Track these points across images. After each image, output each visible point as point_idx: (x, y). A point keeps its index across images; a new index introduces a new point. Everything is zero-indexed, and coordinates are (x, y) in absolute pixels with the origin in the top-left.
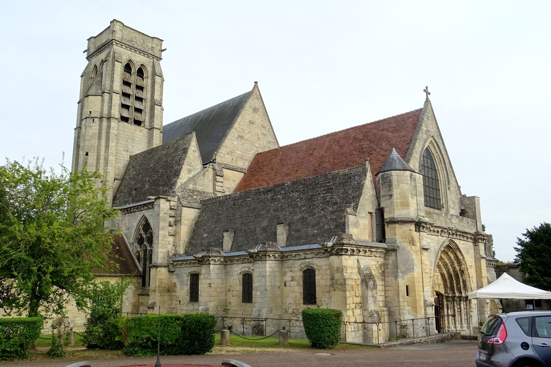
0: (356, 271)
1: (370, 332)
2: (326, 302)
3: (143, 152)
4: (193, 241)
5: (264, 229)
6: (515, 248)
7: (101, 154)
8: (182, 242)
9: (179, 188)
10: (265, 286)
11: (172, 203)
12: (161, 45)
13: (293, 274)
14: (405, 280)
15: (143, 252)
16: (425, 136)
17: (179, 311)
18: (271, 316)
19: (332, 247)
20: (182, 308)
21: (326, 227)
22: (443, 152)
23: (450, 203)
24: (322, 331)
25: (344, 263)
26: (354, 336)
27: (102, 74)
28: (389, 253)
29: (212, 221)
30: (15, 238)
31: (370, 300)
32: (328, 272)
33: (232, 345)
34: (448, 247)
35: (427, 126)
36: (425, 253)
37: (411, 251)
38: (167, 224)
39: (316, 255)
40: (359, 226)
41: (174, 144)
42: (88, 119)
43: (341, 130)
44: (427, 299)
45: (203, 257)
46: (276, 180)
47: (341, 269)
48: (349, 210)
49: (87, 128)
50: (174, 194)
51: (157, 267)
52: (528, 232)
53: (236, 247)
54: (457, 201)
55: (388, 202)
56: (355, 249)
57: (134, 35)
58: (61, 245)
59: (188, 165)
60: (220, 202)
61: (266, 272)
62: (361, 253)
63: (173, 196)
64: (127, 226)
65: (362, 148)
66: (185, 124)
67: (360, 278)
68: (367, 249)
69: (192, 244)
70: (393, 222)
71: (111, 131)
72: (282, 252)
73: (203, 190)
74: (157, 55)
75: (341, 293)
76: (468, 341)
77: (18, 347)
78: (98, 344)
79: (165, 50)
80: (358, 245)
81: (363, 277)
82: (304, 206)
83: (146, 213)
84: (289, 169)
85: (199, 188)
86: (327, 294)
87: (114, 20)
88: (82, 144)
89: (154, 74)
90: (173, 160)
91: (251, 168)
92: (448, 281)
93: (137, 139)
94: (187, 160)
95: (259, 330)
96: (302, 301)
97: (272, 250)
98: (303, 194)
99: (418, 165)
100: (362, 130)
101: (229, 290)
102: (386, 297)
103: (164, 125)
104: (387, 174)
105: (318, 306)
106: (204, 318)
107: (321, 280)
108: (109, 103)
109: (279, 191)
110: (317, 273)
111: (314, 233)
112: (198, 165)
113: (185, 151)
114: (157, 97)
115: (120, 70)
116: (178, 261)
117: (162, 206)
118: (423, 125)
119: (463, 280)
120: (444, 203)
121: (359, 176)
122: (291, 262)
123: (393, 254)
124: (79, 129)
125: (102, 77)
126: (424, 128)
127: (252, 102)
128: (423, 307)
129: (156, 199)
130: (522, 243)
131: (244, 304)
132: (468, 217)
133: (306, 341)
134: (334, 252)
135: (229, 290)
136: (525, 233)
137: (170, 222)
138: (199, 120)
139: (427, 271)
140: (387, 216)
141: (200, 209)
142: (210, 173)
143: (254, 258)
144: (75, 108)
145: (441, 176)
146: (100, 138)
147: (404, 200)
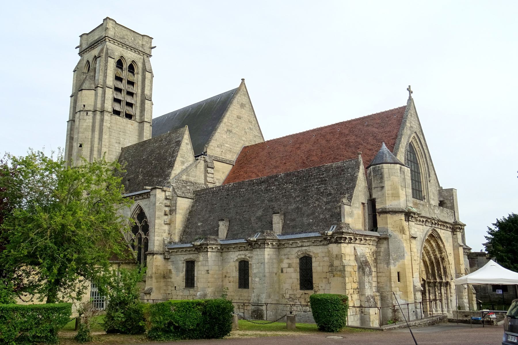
0: (353, 258)
1: (368, 316)
2: (323, 288)
3: (135, 145)
4: (187, 230)
5: (259, 219)
6: (486, 237)
7: (95, 146)
8: (177, 231)
9: (173, 179)
10: (264, 273)
11: (168, 194)
12: (151, 42)
13: (289, 261)
14: (396, 267)
15: (137, 240)
16: (409, 132)
17: (174, 297)
18: (269, 301)
19: (332, 236)
20: (177, 294)
21: (321, 216)
22: (424, 147)
23: (431, 194)
24: (327, 315)
25: (343, 251)
26: (353, 320)
27: (95, 69)
28: (381, 241)
29: (206, 211)
30: (39, 226)
31: (367, 285)
32: (326, 259)
33: (241, 329)
34: (431, 236)
35: (410, 123)
36: (414, 241)
37: (402, 240)
38: (163, 213)
39: (313, 243)
40: (354, 216)
41: (167, 137)
42: (82, 113)
43: (326, 125)
44: (416, 284)
45: (201, 245)
46: (265, 172)
47: (340, 257)
48: (345, 201)
49: (81, 121)
50: (169, 185)
51: (153, 254)
52: (498, 222)
53: (231, 234)
54: (436, 193)
55: (379, 193)
56: (352, 237)
57: (125, 32)
58: (84, 232)
59: (182, 157)
60: (213, 193)
61: (264, 259)
62: (357, 242)
63: (168, 187)
64: (125, 214)
65: (348, 142)
66: (173, 118)
67: (357, 265)
68: (362, 238)
69: (187, 231)
70: (385, 212)
71: (104, 124)
72: (279, 240)
73: (195, 181)
74: (148, 52)
75: (340, 279)
76: (456, 324)
77: (48, 332)
78: (120, 329)
79: (155, 47)
80: (356, 234)
81: (360, 264)
82: (298, 196)
83: (141, 203)
84: (277, 161)
85: (192, 179)
86: (324, 280)
87: (107, 18)
88: (75, 136)
89: (144, 70)
90: (166, 152)
91: (238, 160)
92: (430, 267)
93: (129, 132)
94: (180, 152)
95: (258, 315)
96: (298, 287)
97: (270, 238)
98: (297, 185)
99: (403, 158)
100: (347, 125)
101: (226, 277)
102: (378, 283)
103: (153, 118)
104: (379, 167)
105: (315, 292)
106: (223, 303)
107: (318, 267)
108: (102, 97)
109: (273, 183)
110: (313, 260)
111: (309, 222)
112: (191, 158)
113: (178, 143)
114: (147, 92)
115: (111, 65)
116: (174, 249)
117: (158, 196)
118: (407, 121)
119: (443, 267)
120: (425, 194)
121: (352, 168)
122: (288, 249)
123: (385, 242)
124: (72, 121)
125: (95, 72)
126: (408, 124)
127: (240, 98)
128: (413, 292)
129: (152, 189)
130: (492, 232)
131: (240, 289)
132: (447, 207)
133: (315, 325)
134: (333, 240)
135: (226, 277)
136: (495, 223)
137: (165, 211)
138: (187, 115)
139: (416, 258)
140: (378, 206)
141: (193, 199)
142: (201, 164)
143: (252, 245)
144: (68, 101)
145: (423, 169)
146: (93, 131)
147: (395, 192)
